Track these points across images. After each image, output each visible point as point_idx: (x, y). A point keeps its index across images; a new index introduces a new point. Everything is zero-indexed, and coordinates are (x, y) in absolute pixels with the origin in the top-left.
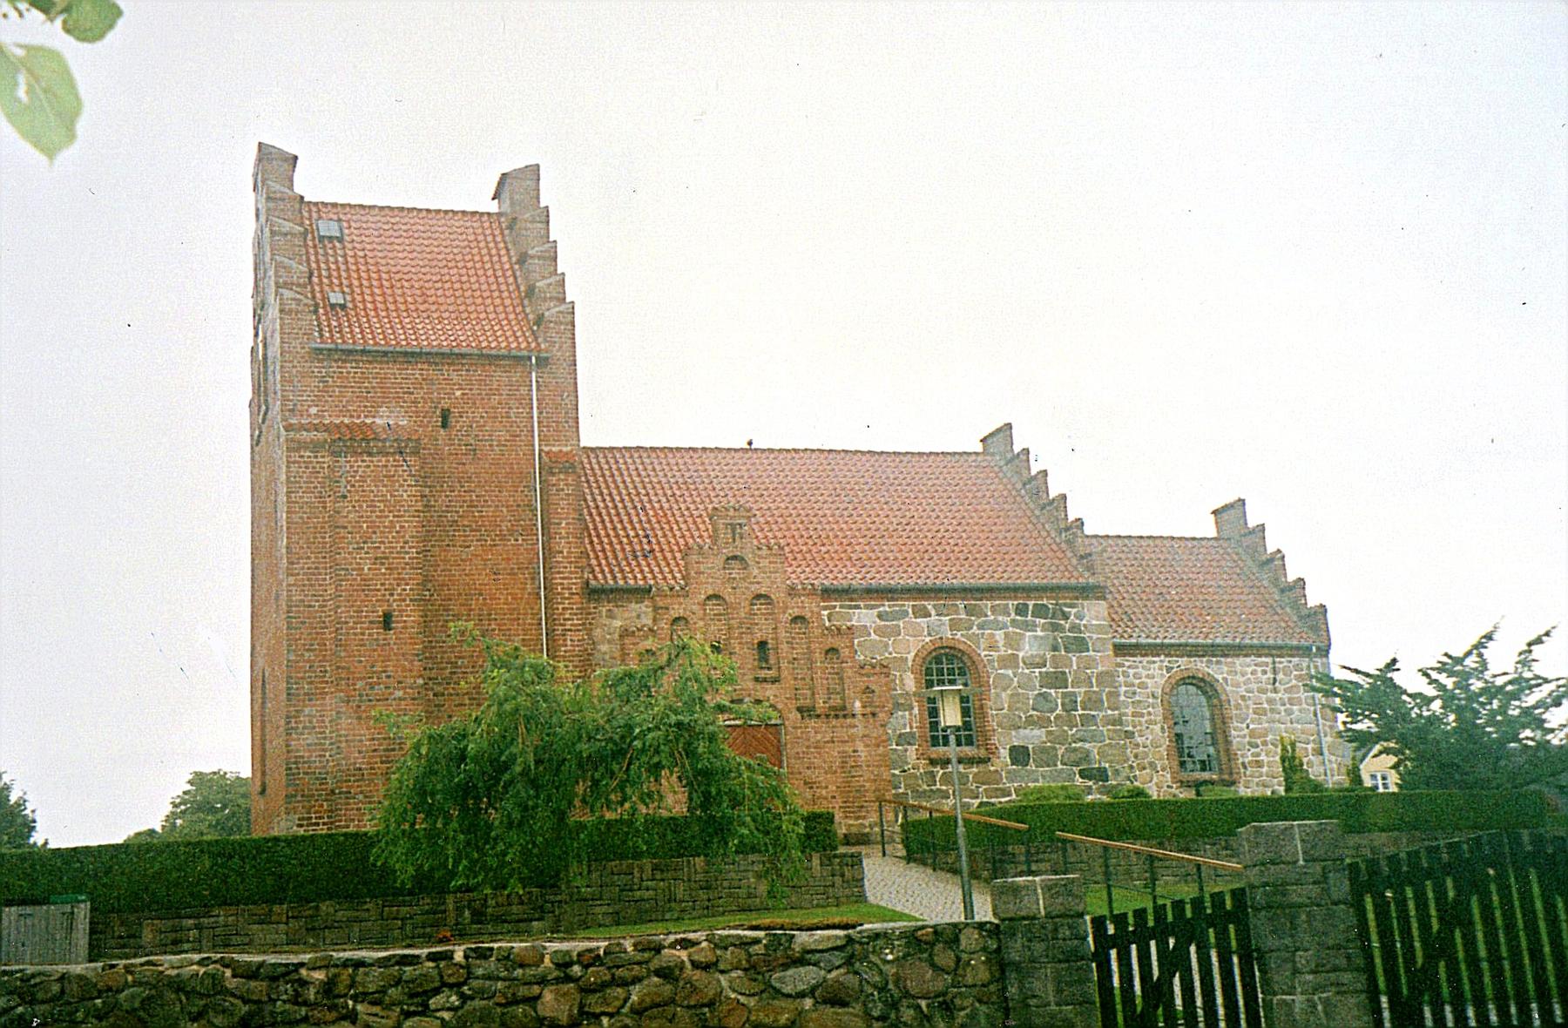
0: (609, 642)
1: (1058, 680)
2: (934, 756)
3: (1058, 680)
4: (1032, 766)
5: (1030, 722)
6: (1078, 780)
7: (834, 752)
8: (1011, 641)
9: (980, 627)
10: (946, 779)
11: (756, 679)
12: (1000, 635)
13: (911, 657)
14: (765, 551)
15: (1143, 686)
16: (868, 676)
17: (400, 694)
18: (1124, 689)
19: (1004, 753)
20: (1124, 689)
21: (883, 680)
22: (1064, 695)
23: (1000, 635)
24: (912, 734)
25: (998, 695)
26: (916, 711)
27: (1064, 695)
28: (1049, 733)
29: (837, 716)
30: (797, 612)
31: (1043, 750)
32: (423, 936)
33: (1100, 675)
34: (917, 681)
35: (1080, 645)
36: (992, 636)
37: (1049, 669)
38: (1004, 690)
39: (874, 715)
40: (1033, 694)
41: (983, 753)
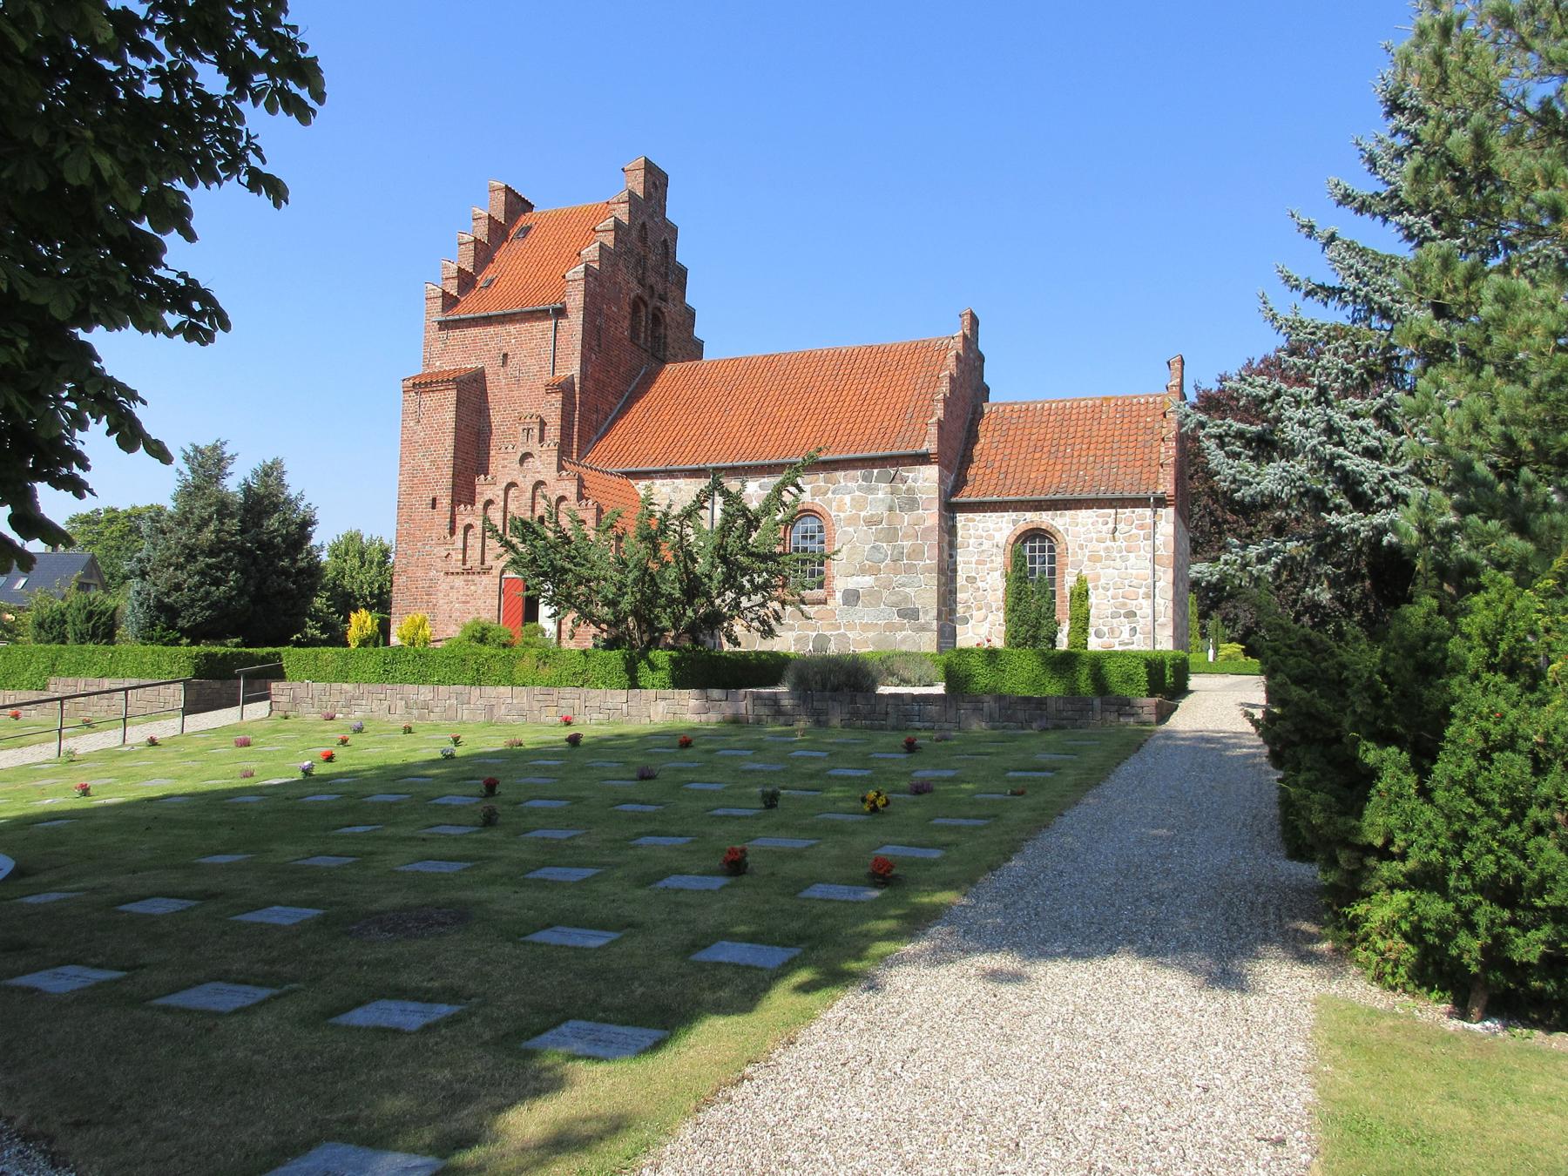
1: (892, 534)
5: (863, 571)
6: (896, 619)
12: (847, 499)
19: (839, 595)
23: (847, 499)
35: (912, 503)
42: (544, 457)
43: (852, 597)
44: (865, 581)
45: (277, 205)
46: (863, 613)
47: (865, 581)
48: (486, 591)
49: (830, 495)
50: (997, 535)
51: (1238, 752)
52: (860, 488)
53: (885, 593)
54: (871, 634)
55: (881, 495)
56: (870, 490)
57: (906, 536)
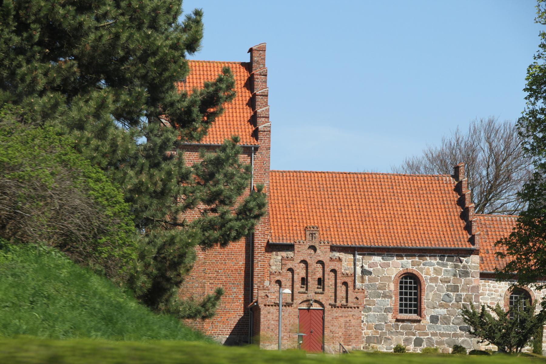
0: (276, 265)
1: (455, 289)
2: (399, 318)
3: (455, 289)
4: (439, 324)
5: (441, 306)
6: (459, 331)
7: (342, 320)
8: (436, 271)
9: (424, 265)
10: (403, 328)
11: (316, 293)
12: (431, 269)
13: (393, 276)
14: (322, 244)
15: (496, 291)
16: (357, 292)
17: (197, 285)
18: (488, 292)
19: (428, 318)
20: (488, 292)
21: (362, 294)
22: (457, 295)
23: (431, 269)
24: (391, 308)
25: (428, 294)
26: (393, 298)
27: (457, 295)
28: (449, 311)
29: (345, 308)
30: (333, 267)
31: (445, 318)
32: (482, 260)
33: (473, 287)
34: (396, 286)
35: (466, 274)
36: (429, 269)
37: (451, 284)
38: (431, 292)
39: (358, 308)
40: (443, 294)
41: (419, 318)
42: (322, 248)
43: (434, 319)
44: (442, 311)
45: (262, 49)
46: (441, 328)
47: (442, 311)
48: (289, 315)
49: (422, 266)
50: (500, 290)
51: (24, 354)
52: (438, 264)
53: (453, 318)
54: (445, 339)
55: (449, 268)
56: (445, 265)
57: (463, 290)
